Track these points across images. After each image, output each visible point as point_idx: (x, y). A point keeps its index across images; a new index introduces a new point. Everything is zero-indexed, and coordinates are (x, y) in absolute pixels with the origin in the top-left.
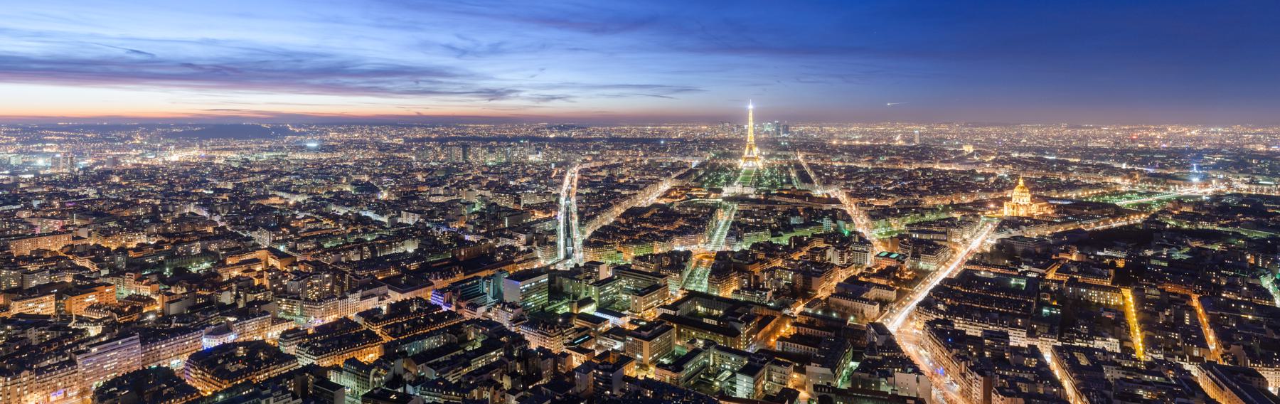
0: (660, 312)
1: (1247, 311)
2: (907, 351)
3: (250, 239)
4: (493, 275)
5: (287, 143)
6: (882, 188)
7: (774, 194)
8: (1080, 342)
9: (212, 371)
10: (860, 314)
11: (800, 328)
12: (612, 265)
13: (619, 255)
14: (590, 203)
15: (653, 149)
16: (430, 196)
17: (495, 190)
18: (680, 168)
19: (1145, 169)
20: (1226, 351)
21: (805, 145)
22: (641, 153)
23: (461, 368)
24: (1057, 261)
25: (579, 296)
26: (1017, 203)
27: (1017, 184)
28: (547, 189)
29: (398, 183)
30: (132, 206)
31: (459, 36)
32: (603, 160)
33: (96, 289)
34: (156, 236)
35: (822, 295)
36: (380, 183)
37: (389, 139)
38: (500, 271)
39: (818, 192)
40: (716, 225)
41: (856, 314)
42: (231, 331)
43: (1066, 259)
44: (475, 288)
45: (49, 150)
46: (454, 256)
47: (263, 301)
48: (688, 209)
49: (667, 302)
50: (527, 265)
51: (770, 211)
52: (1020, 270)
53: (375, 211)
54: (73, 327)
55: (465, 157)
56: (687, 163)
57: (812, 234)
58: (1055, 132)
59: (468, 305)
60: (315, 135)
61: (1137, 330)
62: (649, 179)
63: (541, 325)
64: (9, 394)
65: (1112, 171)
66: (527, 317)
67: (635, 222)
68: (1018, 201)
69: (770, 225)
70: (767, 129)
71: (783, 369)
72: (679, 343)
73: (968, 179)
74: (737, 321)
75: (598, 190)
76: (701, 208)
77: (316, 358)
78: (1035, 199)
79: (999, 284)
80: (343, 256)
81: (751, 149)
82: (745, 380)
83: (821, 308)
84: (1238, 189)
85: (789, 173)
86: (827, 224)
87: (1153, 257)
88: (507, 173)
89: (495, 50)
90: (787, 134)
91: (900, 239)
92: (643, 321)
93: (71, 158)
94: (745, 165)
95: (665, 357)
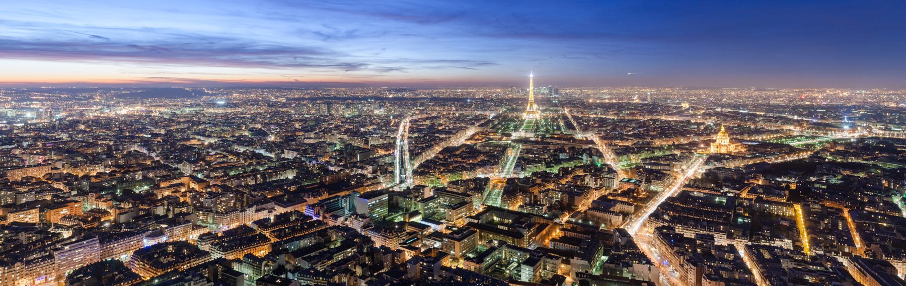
0: (467, 221)
1: (883, 220)
2: (642, 249)
3: (177, 169)
4: (349, 195)
5: (203, 101)
6: (625, 133)
7: (548, 138)
8: (764, 242)
9: (150, 263)
10: (608, 222)
11: (566, 232)
12: (433, 187)
13: (438, 181)
14: (418, 144)
15: (462, 106)
16: (304, 138)
17: (350, 134)
18: (482, 119)
19: (810, 120)
20: (867, 248)
21: (570, 103)
22: (454, 108)
23: (326, 260)
24: (748, 185)
25: (410, 209)
26: (720, 144)
27: (720, 130)
28: (387, 134)
29: (282, 129)
30: (93, 146)
31: (325, 26)
32: (427, 113)
33: (68, 204)
34: (110, 167)
35: (582, 209)
36: (269, 129)
37: (276, 98)
38: (354, 192)
39: (579, 136)
40: (507, 159)
41: (606, 222)
42: (164, 234)
43: (754, 184)
44: (336, 204)
45: (35, 106)
46: (321, 181)
47: (186, 213)
48: (487, 148)
49: (472, 214)
50: (373, 188)
51: (545, 149)
52: (722, 191)
53: (265, 150)
54: (52, 232)
55: (329, 111)
56: (486, 115)
57: (575, 165)
59: (331, 216)
60: (223, 95)
61: (805, 234)
62: (460, 127)
63: (383, 230)
64: (6, 279)
65: (787, 121)
66: (373, 225)
67: (450, 157)
68: (720, 142)
69: (545, 159)
70: (543, 91)
71: (555, 261)
72: (480, 243)
73: (685, 127)
74: (522, 227)
75: (423, 135)
76: (496, 147)
77: (223, 253)
78: (732, 141)
79: (707, 201)
80: (242, 181)
81: (531, 105)
82: (527, 269)
83: (581, 218)
84: (876, 134)
85: (559, 122)
86: (586, 159)
87: (816, 182)
88: (359, 122)
89: (350, 35)
90: (557, 95)
91: (637, 169)
92: (455, 227)
93: (50, 112)
94: (528, 117)
95: (471, 253)
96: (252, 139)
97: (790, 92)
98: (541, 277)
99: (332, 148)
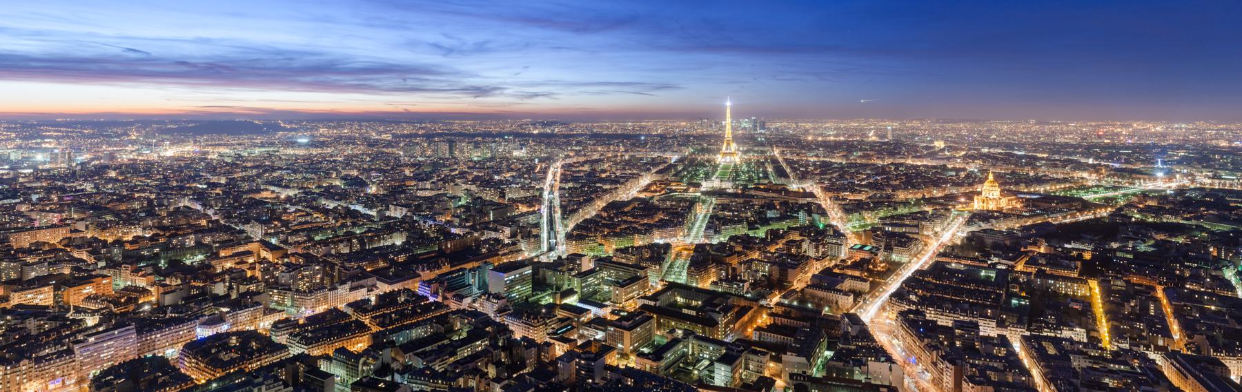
0: (640, 303)
1: (1210, 302)
2: (880, 341)
3: (242, 232)
4: (478, 267)
5: (279, 138)
6: (856, 182)
7: (751, 189)
8: (1048, 332)
9: (206, 360)
10: (834, 305)
11: (776, 318)
12: (593, 257)
13: (600, 248)
14: (573, 197)
15: (634, 145)
16: (417, 190)
17: (480, 184)
18: (660, 163)
19: (1111, 164)
20: (1189, 340)
21: (781, 141)
22: (622, 149)
23: (447, 357)
24: (1026, 253)
25: (562, 287)
26: (987, 197)
27: (987, 178)
28: (531, 183)
29: (387, 177)
30: (128, 200)
31: (445, 35)
32: (585, 155)
33: (93, 280)
34: (151, 229)
35: (798, 286)
36: (369, 177)
37: (378, 135)
38: (486, 263)
39: (794, 186)
40: (695, 218)
41: (831, 304)
42: (225, 321)
43: (1034, 252)
44: (461, 279)
45: (48, 146)
46: (440, 249)
47: (255, 292)
48: (668, 203)
49: (647, 293)
50: (511, 257)
51: (748, 204)
52: (989, 262)
53: (363, 205)
54: (71, 318)
55: (451, 153)
56: (667, 158)
57: (788, 227)
59: (454, 296)
60: (306, 131)
61: (1104, 320)
62: (630, 174)
63: (525, 315)
64: (8, 382)
65: (1079, 166)
66: (511, 308)
67: (616, 215)
68: (987, 195)
69: (747, 218)
70: (744, 125)
71: (760, 358)
72: (658, 333)
73: (940, 173)
74: (716, 312)
75: (580, 185)
76: (680, 202)
77: (306, 347)
78: (1004, 193)
79: (970, 276)
80: (332, 248)
81: (728, 144)
82: (723, 369)
83: (797, 299)
84: (1201, 184)
85: (766, 168)
86: (803, 218)
87: (1119, 249)
88: (492, 167)
89: (480, 48)
90: (764, 130)
91: (873, 232)
92: (624, 311)
93: (69, 153)
94: (723, 160)
96: (346, 190)
97: (1082, 127)
98: (741, 379)
99: (455, 203)
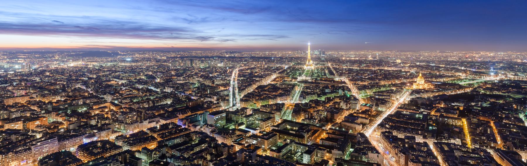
0: (272, 128)
1: (513, 128)
2: (373, 144)
3: (103, 98)
4: (203, 113)
5: (118, 59)
6: (363, 77)
7: (319, 80)
8: (445, 141)
9: (87, 153)
10: (354, 129)
11: (329, 135)
12: (252, 109)
13: (255, 105)
14: (243, 84)
15: (269, 61)
16: (177, 80)
17: (204, 78)
18: (280, 69)
19: (471, 69)
20: (505, 144)
21: (331, 60)
22: (264, 63)
23: (190, 151)
24: (435, 107)
25: (239, 122)
26: (419, 84)
27: (419, 75)
28: (225, 78)
29: (164, 75)
30: (54, 85)
31: (189, 15)
32: (248, 66)
33: (40, 119)
34: (64, 97)
35: (339, 121)
36: (156, 75)
37: (160, 57)
38: (206, 111)
39: (337, 79)
40: (295, 92)
41: (352, 129)
42: (95, 136)
43: (439, 107)
44: (195, 118)
45: (20, 62)
46: (187, 105)
47: (108, 124)
48: (283, 86)
49: (275, 124)
50: (217, 109)
51: (317, 87)
52: (420, 111)
53: (154, 87)
54: (30, 134)
55: (191, 65)
56: (283, 67)
57: (335, 96)
58: (434, 54)
59: (193, 125)
60: (130, 55)
61: (468, 136)
62: (267, 74)
63: (223, 133)
64: (4, 162)
65: (458, 70)
66: (217, 130)
67: (262, 91)
68: (419, 83)
69: (317, 92)
70: (316, 53)
71: (323, 152)
72: (279, 141)
73: (399, 73)
74: (304, 132)
75: (246, 78)
76: (289, 85)
77: (130, 147)
78: (426, 82)
79: (411, 117)
80: (141, 105)
81: (309, 61)
82: (307, 156)
83: (338, 127)
84: (510, 78)
85: (325, 71)
86: (341, 92)
87: (475, 106)
88: (209, 71)
90: (324, 55)
91: (370, 98)
92: (265, 132)
93: (29, 65)
94: (307, 68)
95: (274, 147)
98: (315, 161)
99: (193, 86)
